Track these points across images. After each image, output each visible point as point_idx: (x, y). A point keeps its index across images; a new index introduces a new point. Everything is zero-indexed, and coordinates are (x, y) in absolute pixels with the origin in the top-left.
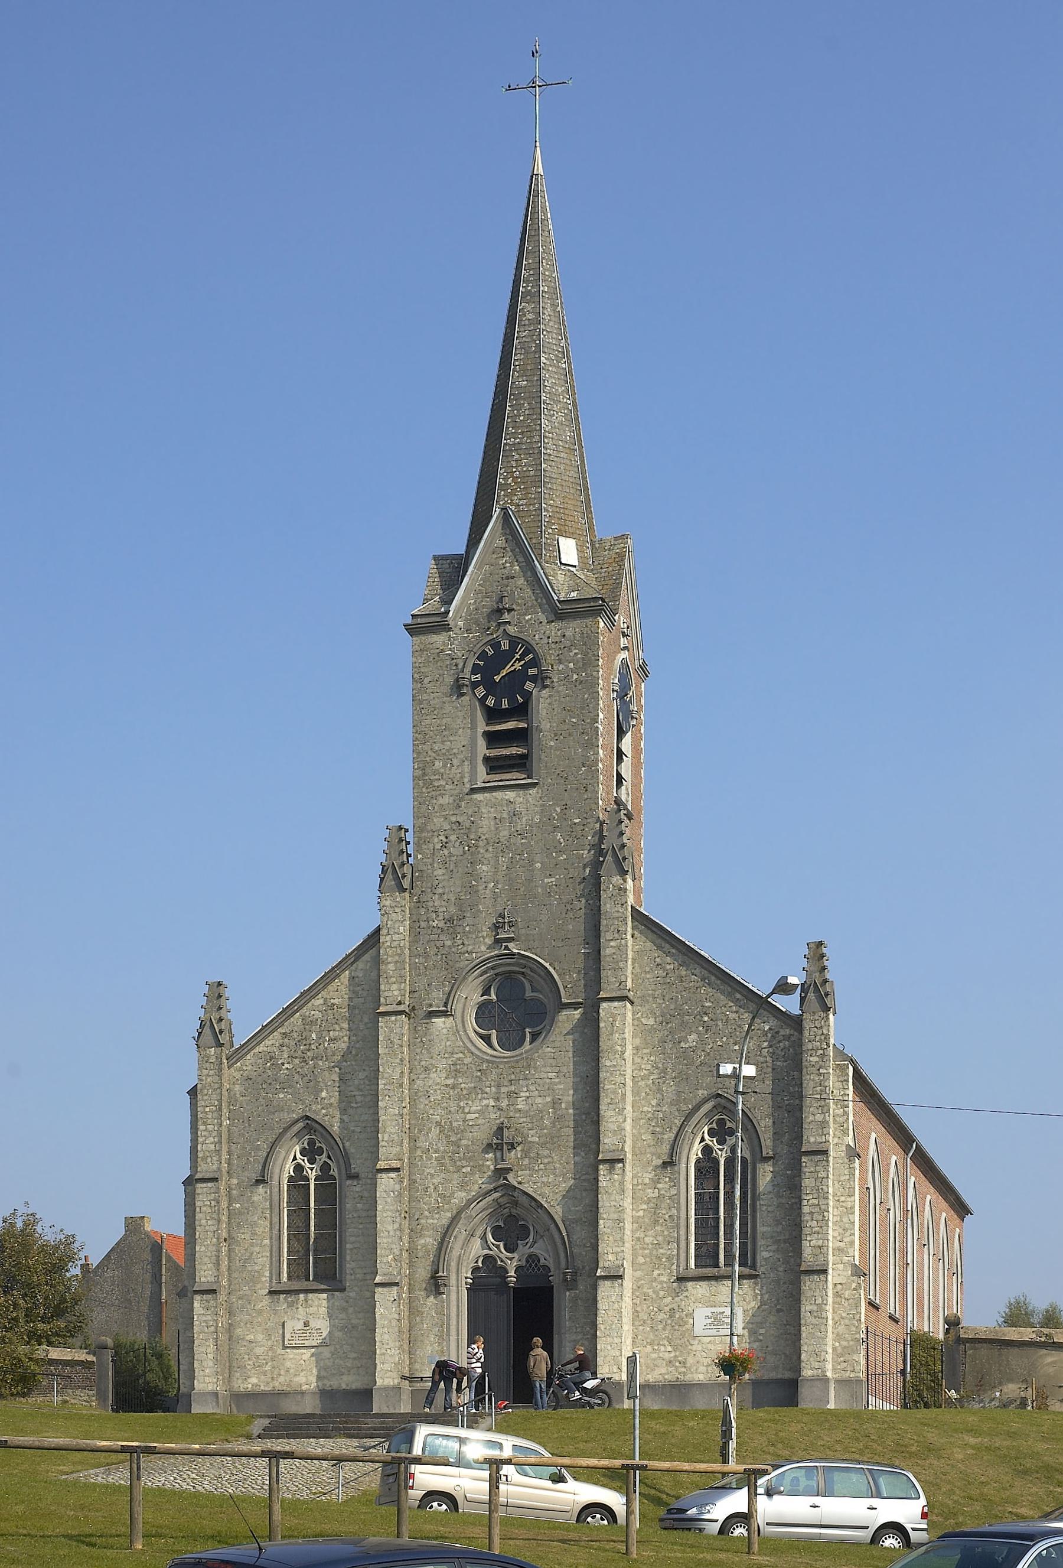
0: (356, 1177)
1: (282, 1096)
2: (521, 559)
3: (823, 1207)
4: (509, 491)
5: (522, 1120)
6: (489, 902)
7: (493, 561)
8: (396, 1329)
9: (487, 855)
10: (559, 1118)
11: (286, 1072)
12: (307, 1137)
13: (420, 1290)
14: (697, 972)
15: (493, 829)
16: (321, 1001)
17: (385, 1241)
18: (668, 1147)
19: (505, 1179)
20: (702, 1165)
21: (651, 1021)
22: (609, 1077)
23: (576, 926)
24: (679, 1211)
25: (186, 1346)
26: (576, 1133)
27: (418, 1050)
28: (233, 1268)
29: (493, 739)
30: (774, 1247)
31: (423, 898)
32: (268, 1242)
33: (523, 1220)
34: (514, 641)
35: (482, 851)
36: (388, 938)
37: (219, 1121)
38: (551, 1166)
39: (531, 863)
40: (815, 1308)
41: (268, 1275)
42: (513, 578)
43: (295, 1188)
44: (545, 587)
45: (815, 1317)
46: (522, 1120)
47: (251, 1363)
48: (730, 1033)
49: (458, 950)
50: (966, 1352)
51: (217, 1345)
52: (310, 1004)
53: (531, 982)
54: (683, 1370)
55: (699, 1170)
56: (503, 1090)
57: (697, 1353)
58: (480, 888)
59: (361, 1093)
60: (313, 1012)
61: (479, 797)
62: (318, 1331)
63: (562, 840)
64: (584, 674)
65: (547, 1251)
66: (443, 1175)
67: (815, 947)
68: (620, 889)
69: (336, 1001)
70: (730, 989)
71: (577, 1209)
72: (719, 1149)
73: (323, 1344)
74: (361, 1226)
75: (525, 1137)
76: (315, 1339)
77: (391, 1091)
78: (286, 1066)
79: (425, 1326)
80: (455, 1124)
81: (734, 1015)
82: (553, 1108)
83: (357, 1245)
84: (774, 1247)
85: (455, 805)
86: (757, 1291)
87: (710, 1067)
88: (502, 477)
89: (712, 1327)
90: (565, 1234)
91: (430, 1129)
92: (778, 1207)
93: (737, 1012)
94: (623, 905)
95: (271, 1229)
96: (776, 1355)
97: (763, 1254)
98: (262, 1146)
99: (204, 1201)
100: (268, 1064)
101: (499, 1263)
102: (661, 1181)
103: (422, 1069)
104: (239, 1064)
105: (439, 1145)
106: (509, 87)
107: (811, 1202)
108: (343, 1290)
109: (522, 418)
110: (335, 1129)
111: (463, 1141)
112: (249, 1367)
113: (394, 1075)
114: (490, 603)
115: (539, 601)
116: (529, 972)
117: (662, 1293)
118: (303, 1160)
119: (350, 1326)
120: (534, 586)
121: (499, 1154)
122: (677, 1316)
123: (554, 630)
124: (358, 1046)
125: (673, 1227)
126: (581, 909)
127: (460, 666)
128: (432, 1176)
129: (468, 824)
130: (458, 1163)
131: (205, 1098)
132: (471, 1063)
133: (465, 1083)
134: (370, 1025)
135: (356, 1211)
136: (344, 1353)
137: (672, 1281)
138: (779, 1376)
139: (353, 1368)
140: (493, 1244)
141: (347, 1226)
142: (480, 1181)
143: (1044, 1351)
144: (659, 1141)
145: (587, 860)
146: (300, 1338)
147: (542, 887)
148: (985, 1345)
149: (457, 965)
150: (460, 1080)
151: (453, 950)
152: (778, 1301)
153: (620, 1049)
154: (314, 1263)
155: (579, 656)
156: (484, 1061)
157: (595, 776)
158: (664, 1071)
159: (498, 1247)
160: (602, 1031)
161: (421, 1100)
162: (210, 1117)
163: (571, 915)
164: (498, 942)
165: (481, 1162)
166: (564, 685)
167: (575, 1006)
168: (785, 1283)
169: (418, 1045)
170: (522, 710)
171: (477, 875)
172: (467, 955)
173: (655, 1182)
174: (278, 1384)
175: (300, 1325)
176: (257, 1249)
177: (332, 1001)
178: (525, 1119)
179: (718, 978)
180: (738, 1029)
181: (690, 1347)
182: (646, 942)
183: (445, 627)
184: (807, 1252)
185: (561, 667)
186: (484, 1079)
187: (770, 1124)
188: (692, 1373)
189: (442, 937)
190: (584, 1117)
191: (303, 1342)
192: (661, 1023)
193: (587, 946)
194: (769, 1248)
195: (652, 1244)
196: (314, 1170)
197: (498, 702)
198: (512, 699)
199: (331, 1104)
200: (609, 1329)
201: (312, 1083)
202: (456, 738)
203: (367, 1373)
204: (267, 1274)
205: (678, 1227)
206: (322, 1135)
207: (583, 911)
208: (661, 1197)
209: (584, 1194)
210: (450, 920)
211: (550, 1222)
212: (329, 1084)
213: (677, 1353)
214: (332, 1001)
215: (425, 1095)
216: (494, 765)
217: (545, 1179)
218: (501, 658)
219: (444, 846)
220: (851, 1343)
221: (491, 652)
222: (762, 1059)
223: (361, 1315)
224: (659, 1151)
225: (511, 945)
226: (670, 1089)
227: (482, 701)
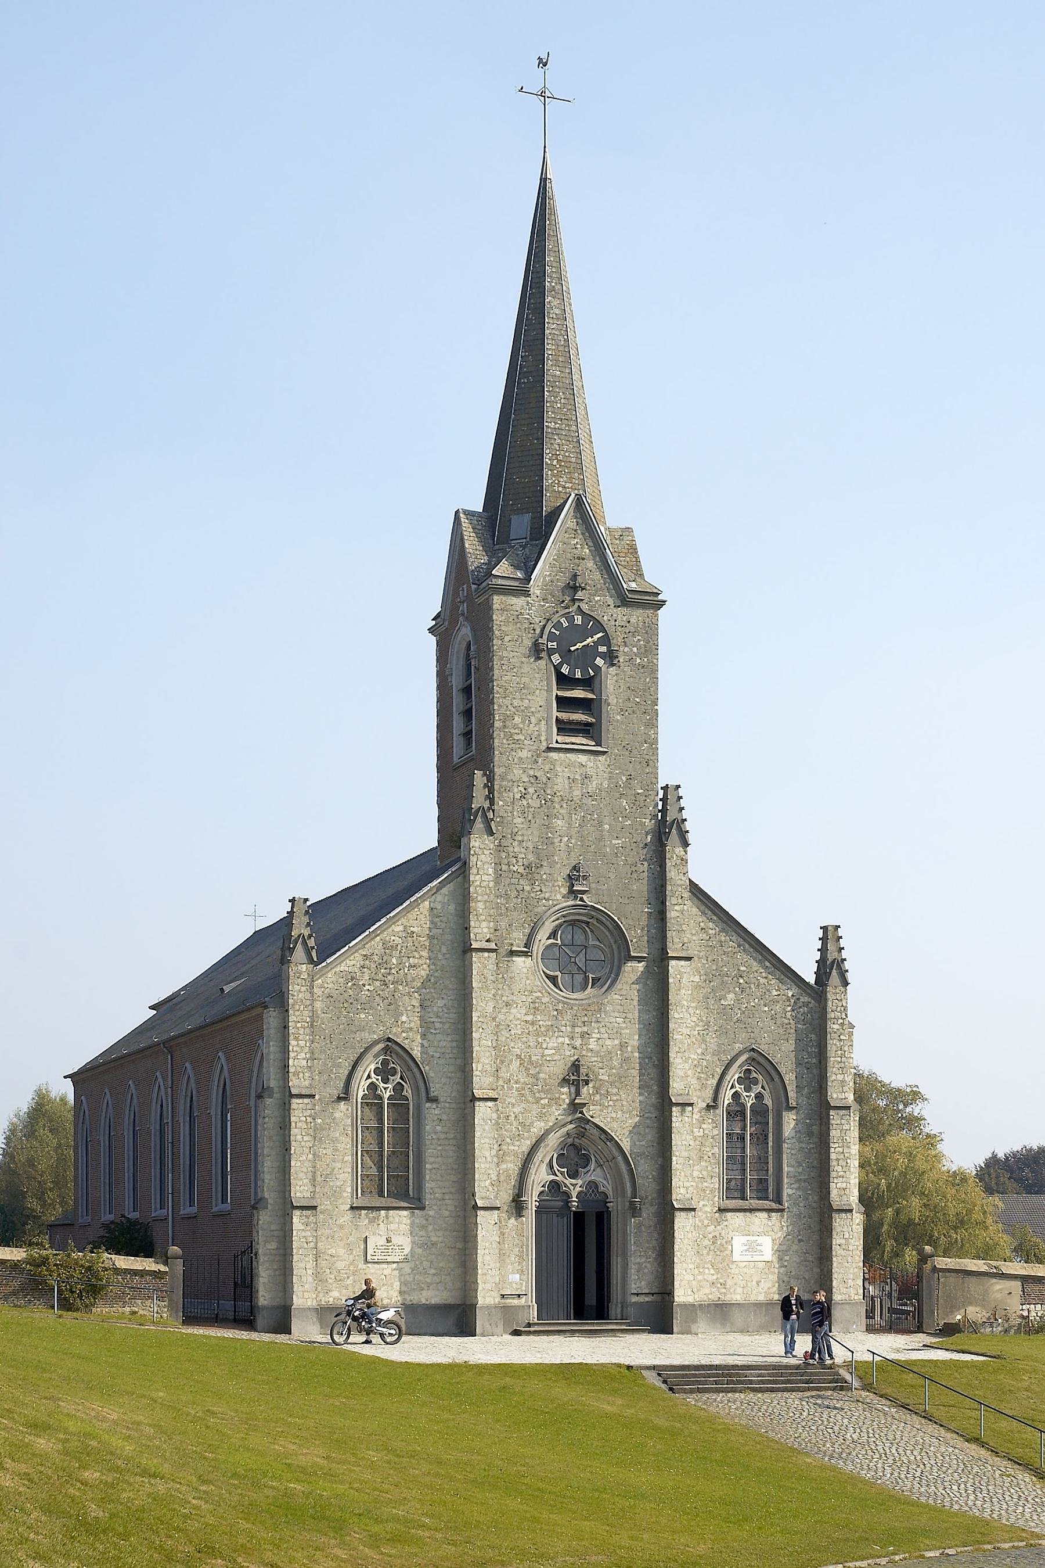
0: (434, 1100)
1: (363, 1016)
2: (591, 544)
3: (846, 1155)
4: (555, 472)
6: (564, 855)
7: (566, 540)
8: (497, 1251)
9: (562, 811)
10: (626, 1060)
11: (367, 993)
12: (382, 1057)
14: (734, 938)
15: (567, 787)
16: (401, 928)
17: (483, 1166)
18: (711, 1092)
21: (697, 979)
22: (677, 1029)
23: (641, 887)
25: (266, 1259)
27: (500, 986)
29: (563, 703)
30: (796, 1186)
31: (504, 843)
35: (557, 806)
37: (311, 1037)
38: (619, 1104)
39: (600, 824)
40: (843, 1241)
41: (350, 1191)
42: (583, 559)
43: (368, 1105)
44: (615, 575)
45: (844, 1249)
46: (593, 1059)
47: (332, 1276)
48: (761, 996)
49: (536, 895)
50: (939, 1279)
51: (316, 1261)
52: (390, 930)
54: (724, 1290)
55: (729, 1113)
57: (735, 1277)
58: (556, 841)
59: (440, 1020)
60: (393, 938)
61: (554, 755)
62: (400, 1248)
63: (627, 807)
64: (646, 660)
65: (606, 1179)
66: (523, 1105)
67: (833, 930)
68: (682, 860)
70: (760, 957)
71: (641, 1143)
72: (747, 1096)
73: (406, 1260)
74: (440, 1148)
75: (596, 1075)
76: (397, 1254)
77: (485, 1024)
78: (367, 987)
79: (506, 1246)
80: (534, 1058)
81: (765, 981)
82: (621, 1050)
84: (796, 1186)
85: (533, 760)
86: (783, 1223)
87: (745, 1024)
88: (548, 457)
89: (747, 1253)
91: (511, 1061)
92: (799, 1151)
93: (766, 978)
94: (684, 874)
96: (798, 1279)
97: (787, 1191)
98: (343, 1064)
99: (300, 1117)
100: (350, 984)
101: (564, 1188)
102: (705, 1121)
103: (504, 1004)
104: (320, 981)
105: (519, 1076)
106: (522, 88)
107: (837, 1149)
108: (423, 1208)
109: (559, 405)
110: (416, 1053)
111: (541, 1075)
113: (487, 1008)
114: (563, 579)
115: (607, 585)
116: (595, 923)
118: (377, 1080)
119: (429, 1244)
120: (602, 570)
121: (573, 1089)
122: (719, 1243)
123: (621, 614)
124: (436, 974)
126: (644, 872)
127: (538, 631)
130: (537, 1095)
131: (297, 1013)
132: (548, 1003)
133: (544, 1021)
134: (447, 956)
135: (436, 1133)
136: (424, 1269)
137: (715, 1211)
139: (432, 1284)
140: (558, 1170)
141: (427, 1147)
142: (557, 1113)
143: (994, 1280)
145: (649, 828)
146: (383, 1254)
147: (610, 847)
148: (953, 1274)
149: (536, 910)
150: (539, 1017)
151: (532, 895)
152: (799, 1232)
153: (686, 1004)
155: (642, 642)
156: (559, 1001)
157: (655, 753)
158: (708, 1024)
159: (562, 1173)
160: (672, 986)
161: (503, 1033)
162: (302, 1033)
163: (635, 875)
164: (572, 892)
166: (629, 666)
167: (639, 959)
168: (804, 1217)
169: (500, 980)
171: (553, 828)
172: (544, 901)
175: (383, 1241)
176: (339, 1165)
177: (412, 929)
178: (596, 1059)
179: (751, 945)
180: (767, 993)
181: (729, 1271)
182: (692, 907)
183: (526, 593)
184: (834, 1194)
185: (626, 650)
186: (560, 1018)
187: (794, 1078)
188: (731, 1294)
189: (522, 882)
190: (647, 1060)
191: (385, 1257)
193: (649, 906)
194: (793, 1186)
195: (698, 1178)
196: (389, 1090)
197: (572, 671)
198: (584, 671)
199: (411, 1029)
200: (685, 1256)
201: (393, 1006)
202: (534, 698)
203: (446, 1289)
204: (349, 1190)
206: (397, 1054)
207: (646, 874)
209: (647, 1131)
210: (528, 867)
211: (616, 1153)
212: (409, 1008)
214: (412, 929)
215: (506, 1029)
222: (787, 1021)
223: (440, 1233)
224: (703, 1095)
225: (585, 897)
226: (712, 1041)
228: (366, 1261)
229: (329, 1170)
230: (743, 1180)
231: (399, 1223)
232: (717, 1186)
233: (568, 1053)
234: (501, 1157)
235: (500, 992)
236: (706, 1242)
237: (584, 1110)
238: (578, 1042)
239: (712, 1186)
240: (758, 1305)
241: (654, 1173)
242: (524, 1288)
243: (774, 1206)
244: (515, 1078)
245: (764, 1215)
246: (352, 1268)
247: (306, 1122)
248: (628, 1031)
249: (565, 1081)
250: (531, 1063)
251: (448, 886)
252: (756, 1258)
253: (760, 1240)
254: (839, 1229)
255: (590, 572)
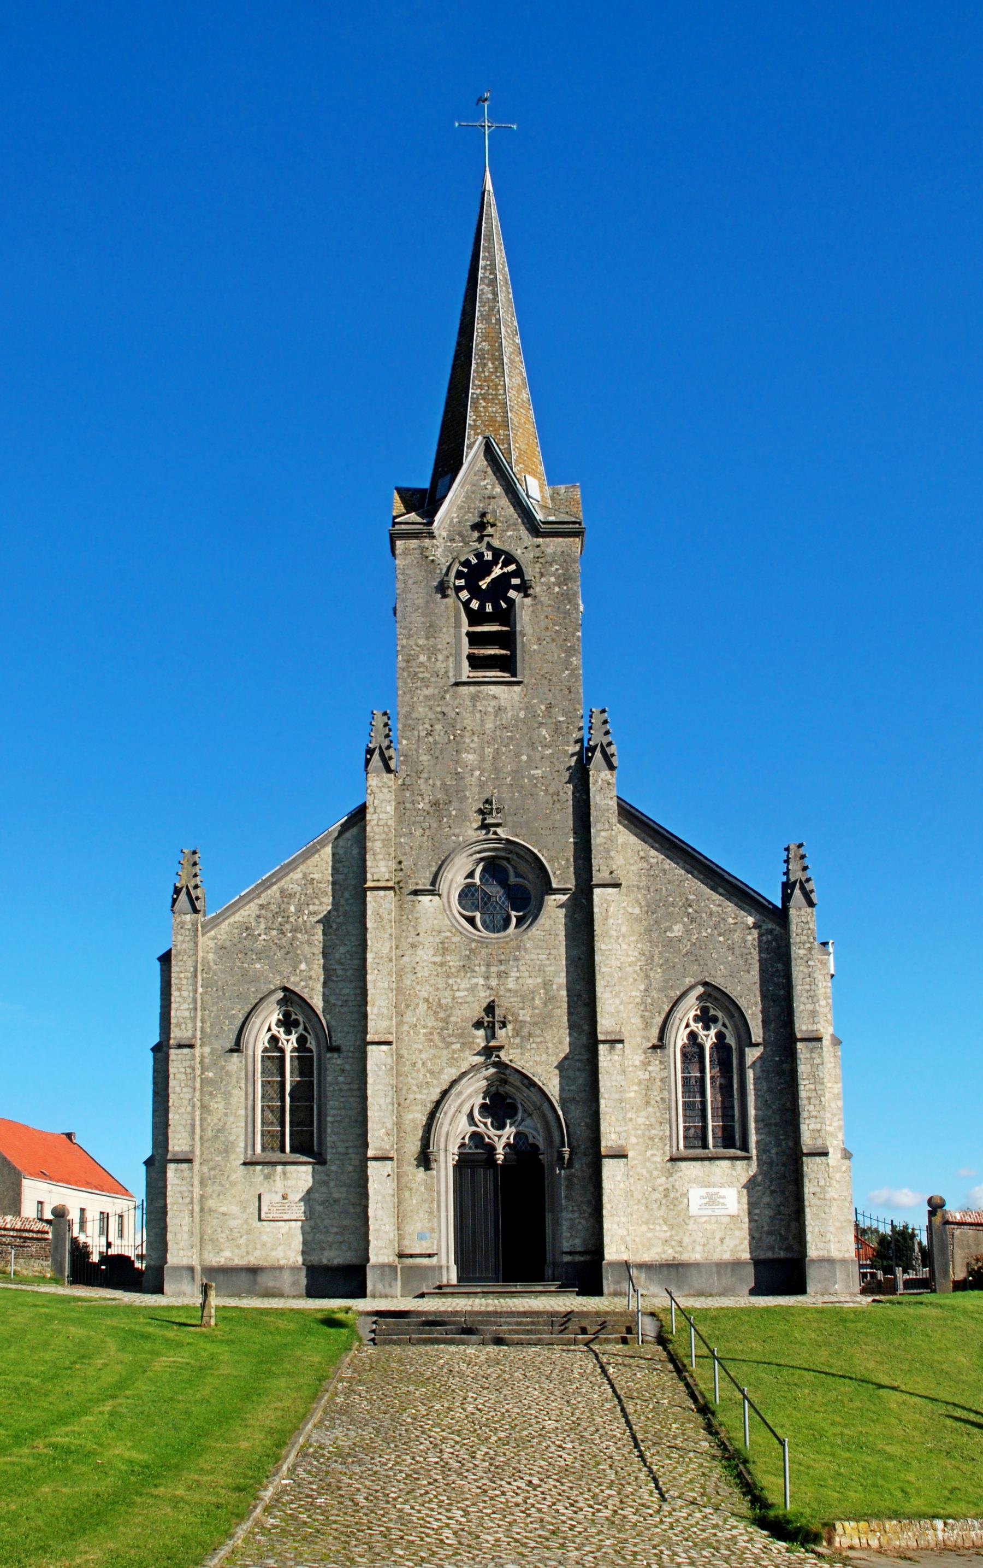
0: (337, 1049)
1: (258, 966)
3: (819, 1092)
5: (512, 1000)
6: (476, 790)
10: (549, 1000)
13: (409, 1165)
16: (300, 876)
17: (376, 1114)
19: (498, 1056)
20: (688, 1050)
24: (670, 1093)
26: (570, 1014)
28: (205, 1138)
29: (475, 639)
31: (408, 781)
32: (242, 1112)
33: (511, 1098)
34: (497, 553)
35: (467, 740)
36: (375, 816)
38: (543, 1046)
42: (494, 498)
46: (512, 1000)
47: (224, 1235)
53: (515, 868)
54: (680, 1249)
56: (493, 969)
57: (694, 1233)
60: (291, 886)
69: (316, 876)
74: (342, 1099)
75: (516, 1016)
80: (443, 1001)
82: (544, 988)
83: (339, 1118)
90: (560, 1113)
91: (417, 1004)
93: (720, 905)
95: (246, 1099)
107: (807, 1087)
110: (318, 1003)
112: (221, 1240)
117: (655, 1173)
121: (489, 1032)
124: (338, 920)
125: (665, 1109)
127: (444, 571)
128: (421, 1051)
129: (453, 715)
131: (180, 964)
134: (350, 901)
135: (337, 1084)
138: (776, 1256)
144: (647, 1025)
154: (291, 1135)
160: (597, 916)
164: (484, 826)
165: (471, 1040)
170: (506, 616)
173: (646, 1064)
174: (253, 1259)
175: (278, 1198)
192: (647, 912)
197: (482, 606)
198: (496, 606)
201: (291, 954)
204: (242, 1144)
205: (669, 1109)
208: (652, 1080)
209: (578, 1074)
210: (436, 804)
213: (673, 1233)
214: (312, 876)
216: (476, 662)
217: (537, 1058)
218: (484, 568)
219: (429, 734)
220: (844, 1224)
221: (474, 561)
222: (747, 951)
223: (344, 1189)
225: (499, 830)
226: (657, 975)
227: (466, 604)
228: (260, 1219)
229: (221, 1124)
230: (704, 1128)
231: (298, 1179)
232: (668, 1133)
233: (483, 994)
234: (400, 1105)
235: (404, 934)
236: (656, 1195)
237: (502, 1054)
238: (494, 982)
239: (661, 1133)
240: (721, 1266)
241: (587, 1120)
242: (435, 1247)
243: (739, 1153)
244: (422, 1023)
245: (726, 1163)
246: (245, 1226)
247: (185, 1073)
248: (553, 968)
249: (478, 1025)
250: (440, 1005)
251: (351, 830)
252: (718, 1212)
253: (722, 1191)
254: (812, 1176)
255: (503, 508)
